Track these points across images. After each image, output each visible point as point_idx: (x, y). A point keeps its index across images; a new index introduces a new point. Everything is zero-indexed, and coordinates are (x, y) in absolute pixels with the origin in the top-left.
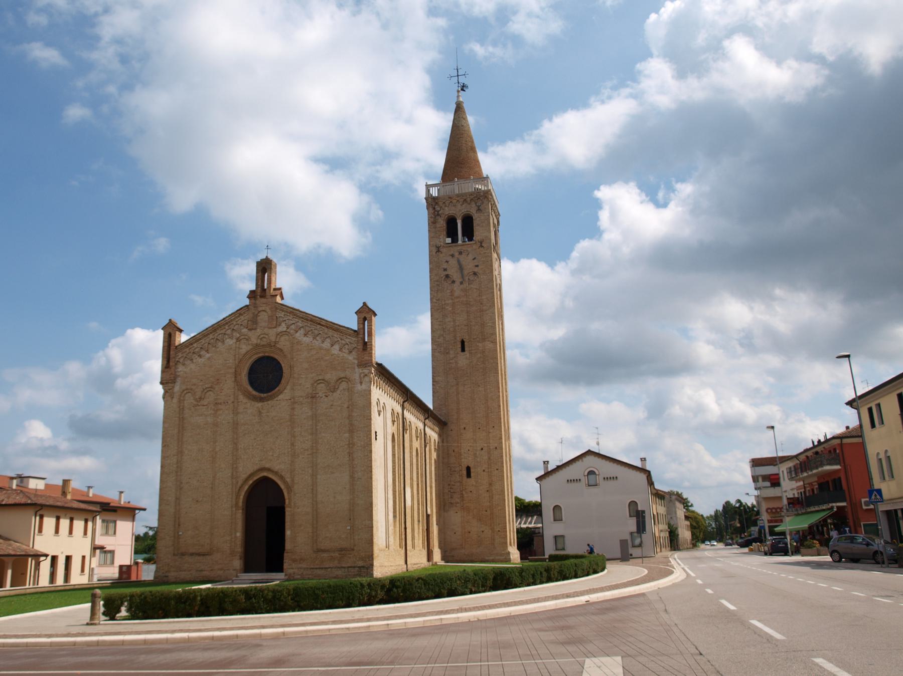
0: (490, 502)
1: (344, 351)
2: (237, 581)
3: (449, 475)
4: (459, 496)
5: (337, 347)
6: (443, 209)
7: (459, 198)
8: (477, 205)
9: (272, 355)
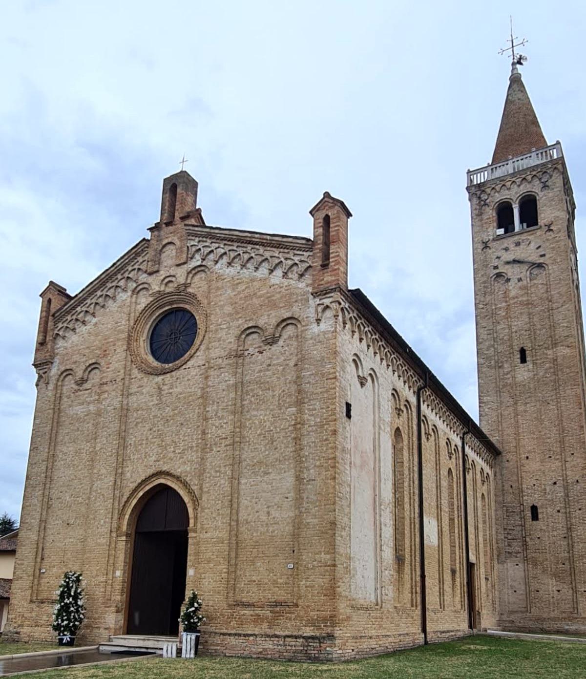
0: (569, 552)
3: (505, 516)
5: (279, 272)
6: (492, 197)
8: (543, 181)
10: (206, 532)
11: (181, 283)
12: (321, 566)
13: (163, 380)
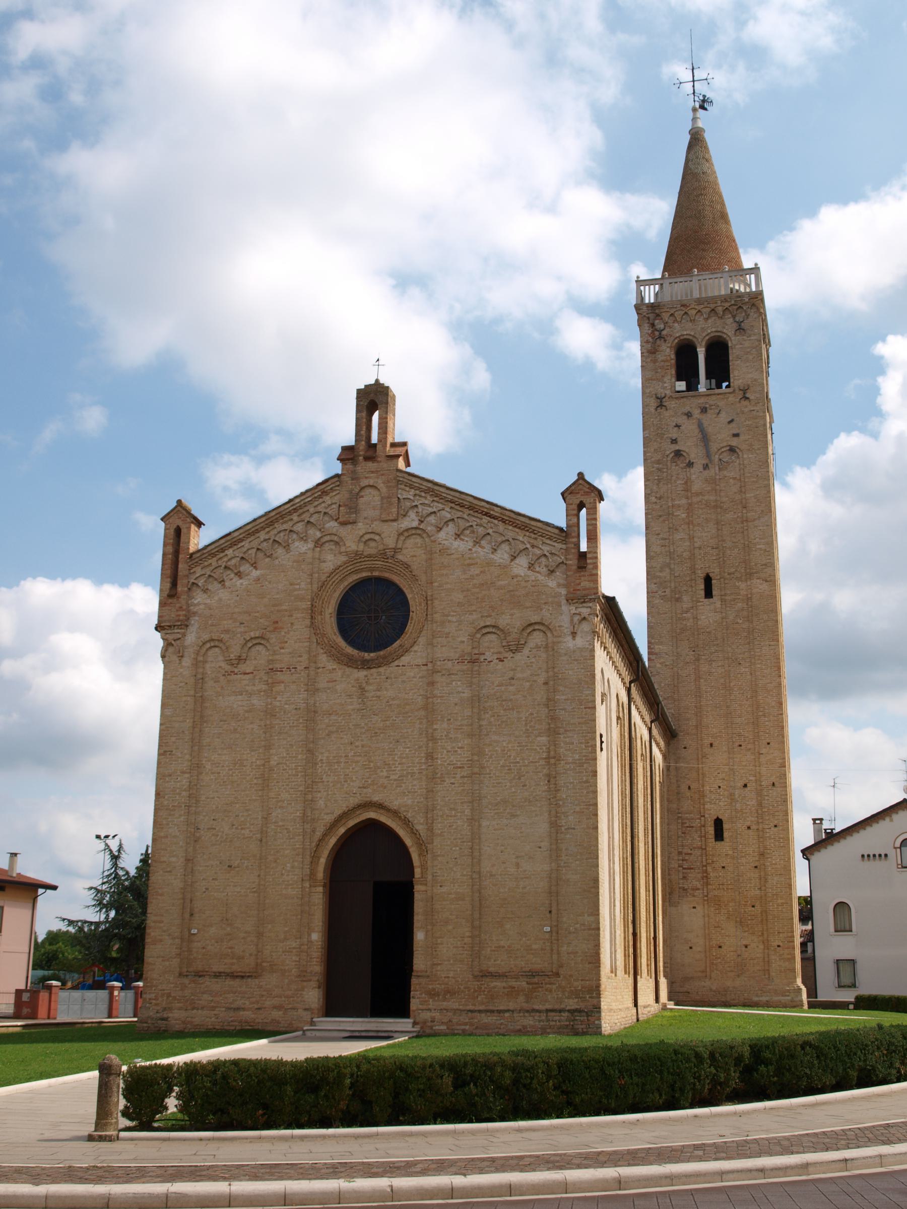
0: (760, 889)
1: (538, 569)
2: (314, 1033)
4: (700, 876)
5: (523, 561)
7: (702, 306)
8: (737, 319)
9: (386, 575)
10: (441, 886)
11: (390, 547)
12: (584, 930)
13: (366, 676)
